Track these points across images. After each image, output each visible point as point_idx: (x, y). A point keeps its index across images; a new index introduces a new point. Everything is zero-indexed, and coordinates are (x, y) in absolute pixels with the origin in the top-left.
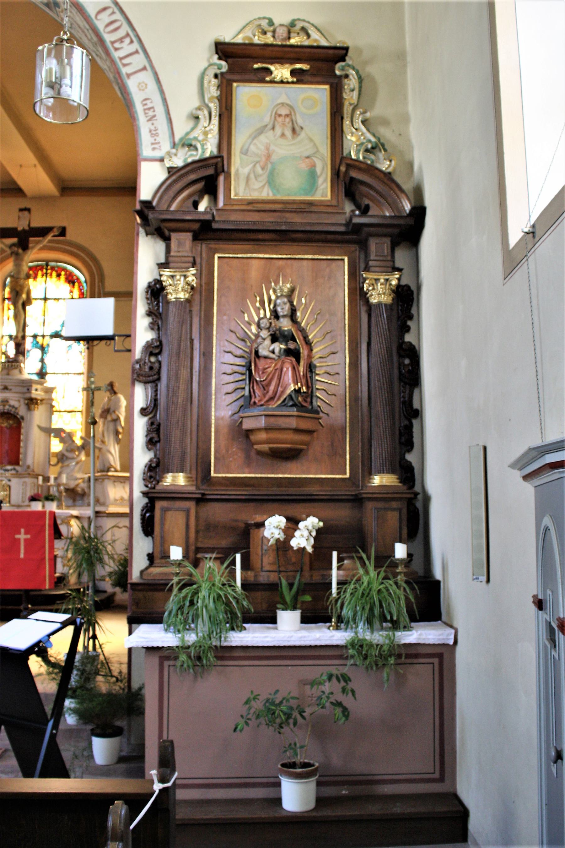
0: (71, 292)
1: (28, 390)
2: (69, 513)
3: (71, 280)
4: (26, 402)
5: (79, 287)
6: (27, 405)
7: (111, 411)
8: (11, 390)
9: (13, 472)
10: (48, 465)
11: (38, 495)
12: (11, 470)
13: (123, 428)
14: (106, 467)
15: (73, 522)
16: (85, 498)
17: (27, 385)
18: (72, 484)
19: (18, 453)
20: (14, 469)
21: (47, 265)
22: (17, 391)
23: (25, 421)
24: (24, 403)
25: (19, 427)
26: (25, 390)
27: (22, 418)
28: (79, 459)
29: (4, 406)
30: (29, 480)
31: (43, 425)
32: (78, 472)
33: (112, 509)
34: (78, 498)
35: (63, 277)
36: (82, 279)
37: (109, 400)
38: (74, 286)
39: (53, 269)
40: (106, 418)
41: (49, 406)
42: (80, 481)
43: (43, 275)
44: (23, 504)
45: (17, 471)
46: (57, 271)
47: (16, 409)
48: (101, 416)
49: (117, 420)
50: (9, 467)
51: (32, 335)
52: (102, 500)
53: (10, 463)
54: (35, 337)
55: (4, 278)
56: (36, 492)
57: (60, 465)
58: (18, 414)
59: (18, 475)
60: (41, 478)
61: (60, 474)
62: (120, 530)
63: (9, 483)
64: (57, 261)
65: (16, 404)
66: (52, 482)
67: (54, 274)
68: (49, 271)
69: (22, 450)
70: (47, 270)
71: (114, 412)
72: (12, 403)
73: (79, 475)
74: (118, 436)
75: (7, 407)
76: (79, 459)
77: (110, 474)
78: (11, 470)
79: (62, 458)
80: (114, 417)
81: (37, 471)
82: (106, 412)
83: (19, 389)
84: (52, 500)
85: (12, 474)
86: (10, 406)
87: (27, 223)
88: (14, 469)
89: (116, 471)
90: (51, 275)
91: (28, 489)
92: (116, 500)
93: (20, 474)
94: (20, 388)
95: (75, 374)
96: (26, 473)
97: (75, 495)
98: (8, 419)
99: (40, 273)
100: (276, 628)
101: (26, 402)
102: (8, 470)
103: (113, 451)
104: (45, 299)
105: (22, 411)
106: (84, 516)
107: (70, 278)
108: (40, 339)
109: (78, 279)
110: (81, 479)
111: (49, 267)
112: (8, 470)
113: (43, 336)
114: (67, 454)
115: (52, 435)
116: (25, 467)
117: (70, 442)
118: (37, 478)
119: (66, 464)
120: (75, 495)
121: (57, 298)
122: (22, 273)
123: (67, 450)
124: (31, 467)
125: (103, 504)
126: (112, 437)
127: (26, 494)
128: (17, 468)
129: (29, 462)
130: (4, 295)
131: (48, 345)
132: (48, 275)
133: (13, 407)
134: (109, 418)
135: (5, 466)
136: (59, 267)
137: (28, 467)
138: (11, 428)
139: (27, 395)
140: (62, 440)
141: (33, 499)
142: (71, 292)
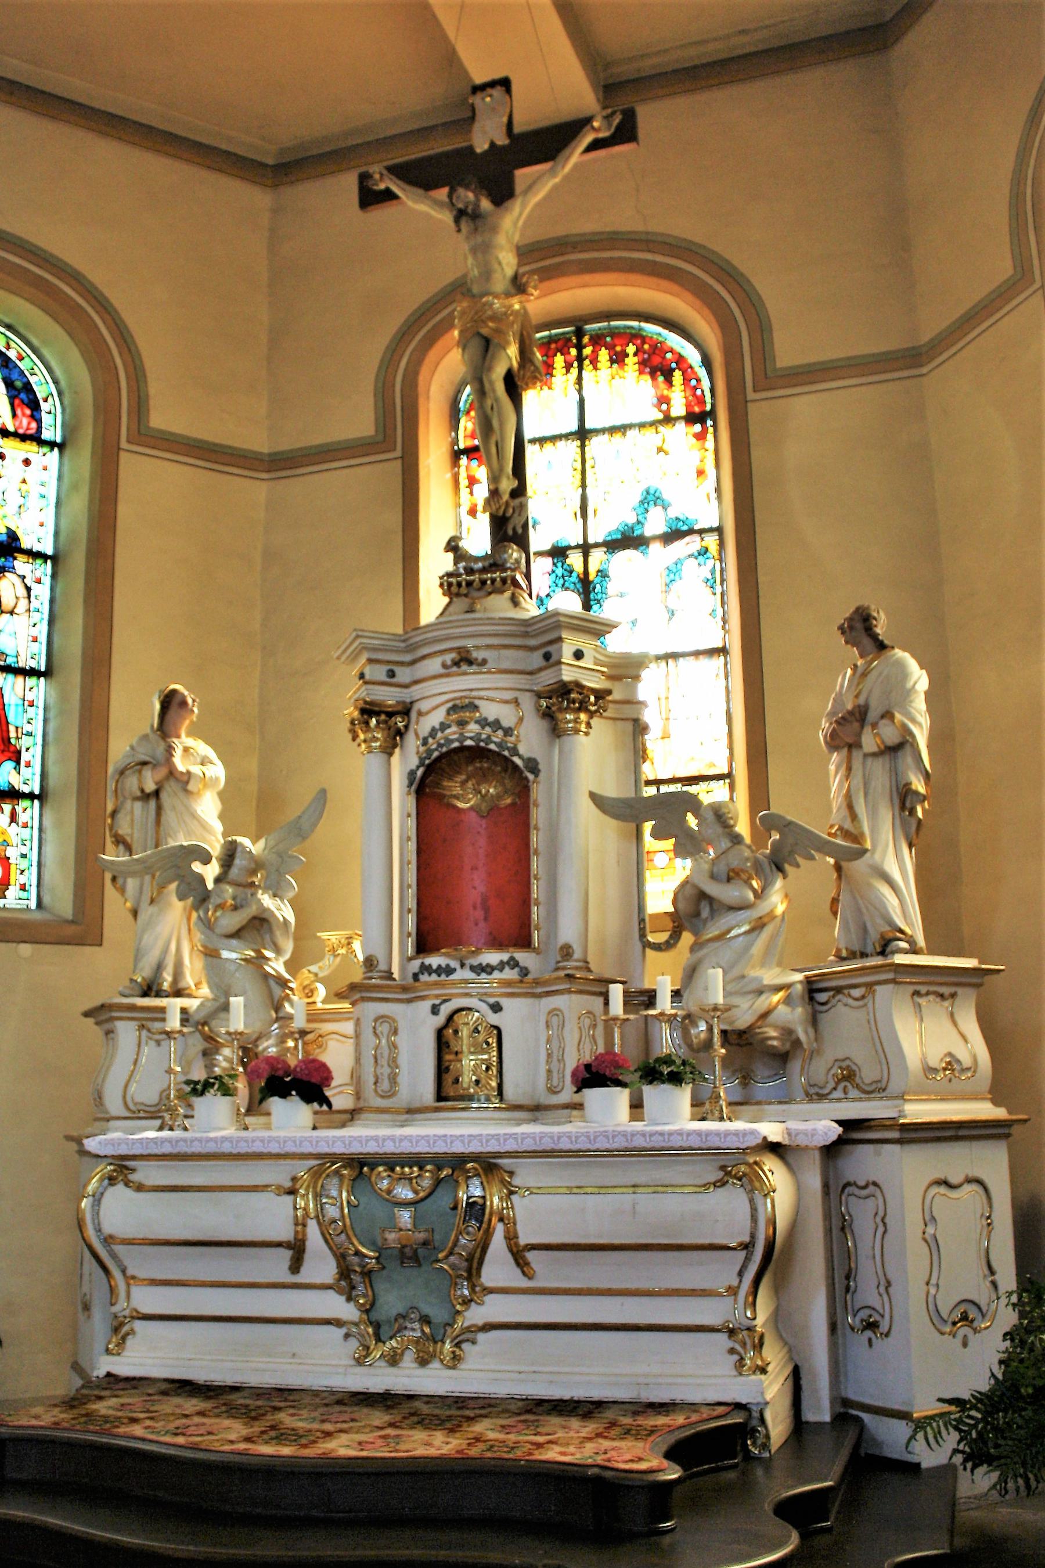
0: (663, 400)
1: (547, 656)
2: (753, 1132)
3: (659, 366)
4: (544, 703)
5: (686, 380)
6: (548, 715)
7: (872, 715)
8: (484, 662)
9: (509, 974)
10: (638, 946)
11: (609, 1058)
12: (501, 967)
13: (927, 776)
14: (874, 935)
15: (775, 1173)
16: (795, 1066)
17: (543, 637)
18: (743, 1017)
19: (525, 902)
20: (513, 963)
21: (579, 333)
22: (506, 665)
23: (542, 776)
24: (538, 707)
25: (523, 790)
26: (536, 660)
27: (533, 766)
28: (763, 908)
29: (462, 723)
30: (572, 1005)
31: (611, 791)
32: (764, 962)
33: (919, 1111)
34: (761, 1070)
35: (631, 361)
36: (693, 356)
37: (861, 675)
38: (669, 382)
39: (597, 340)
40: (854, 745)
41: (629, 726)
42: (776, 998)
43: (568, 367)
44: (555, 1100)
45: (525, 972)
46: (610, 347)
47: (508, 732)
48: (834, 742)
49: (899, 748)
50: (492, 957)
51: (547, 547)
52: (868, 1074)
53: (497, 943)
54: (558, 553)
55: (451, 393)
56: (601, 1050)
57: (687, 938)
58: (515, 751)
59: (529, 986)
60: (616, 992)
61: (691, 973)
62: (954, 1194)
63: (493, 1019)
64: (609, 316)
65: (507, 716)
66: (665, 1004)
67: (604, 354)
68: (587, 351)
69: (537, 890)
70: (580, 347)
71: (888, 715)
72: (490, 710)
73: (771, 976)
74: (912, 812)
75: (473, 728)
76: (763, 908)
77: (900, 959)
78: (501, 967)
79: (695, 909)
80: (889, 734)
81: (599, 967)
82: (850, 727)
83: (510, 658)
84: (676, 1079)
85: (508, 983)
86: (483, 723)
87: (505, 119)
88: (513, 963)
89: (914, 951)
90: (594, 362)
91: (571, 1035)
92: (929, 1070)
93: (537, 982)
94: (521, 653)
95: (697, 654)
96: (562, 973)
97: (754, 1057)
98: (484, 776)
99: (559, 360)
100: (583, 1116)
101: (544, 703)
102: (488, 969)
103: (897, 876)
104: (582, 434)
105: (530, 740)
106: (802, 1141)
107: (656, 360)
108: (575, 560)
109: (680, 359)
110: (778, 988)
111: (586, 340)
112: (488, 969)
113: (586, 549)
114: (713, 889)
115: (648, 826)
116: (555, 956)
117: (725, 844)
118: (606, 996)
119: (712, 932)
120: (754, 1057)
121: (618, 423)
122: (497, 276)
123: (713, 877)
124: (577, 954)
125: (877, 1090)
126: (886, 818)
127: (561, 1060)
128: (523, 957)
129: (568, 932)
130: (455, 441)
131: (603, 574)
132: (587, 362)
133: (496, 725)
134: (869, 742)
135: (477, 952)
136: (614, 333)
137: (566, 952)
138: (491, 812)
139: (547, 679)
140: (687, 845)
141: (592, 1076)
142: (663, 400)
